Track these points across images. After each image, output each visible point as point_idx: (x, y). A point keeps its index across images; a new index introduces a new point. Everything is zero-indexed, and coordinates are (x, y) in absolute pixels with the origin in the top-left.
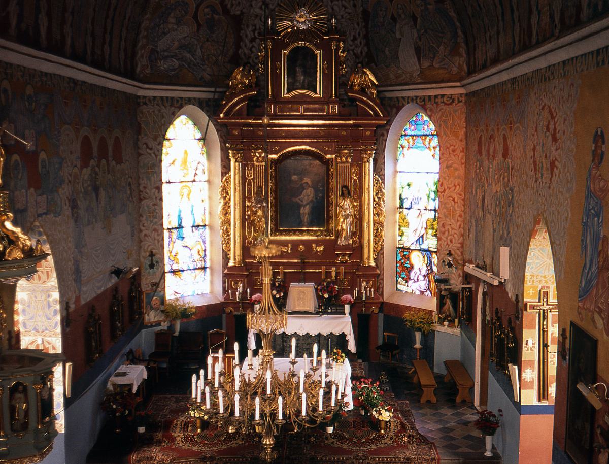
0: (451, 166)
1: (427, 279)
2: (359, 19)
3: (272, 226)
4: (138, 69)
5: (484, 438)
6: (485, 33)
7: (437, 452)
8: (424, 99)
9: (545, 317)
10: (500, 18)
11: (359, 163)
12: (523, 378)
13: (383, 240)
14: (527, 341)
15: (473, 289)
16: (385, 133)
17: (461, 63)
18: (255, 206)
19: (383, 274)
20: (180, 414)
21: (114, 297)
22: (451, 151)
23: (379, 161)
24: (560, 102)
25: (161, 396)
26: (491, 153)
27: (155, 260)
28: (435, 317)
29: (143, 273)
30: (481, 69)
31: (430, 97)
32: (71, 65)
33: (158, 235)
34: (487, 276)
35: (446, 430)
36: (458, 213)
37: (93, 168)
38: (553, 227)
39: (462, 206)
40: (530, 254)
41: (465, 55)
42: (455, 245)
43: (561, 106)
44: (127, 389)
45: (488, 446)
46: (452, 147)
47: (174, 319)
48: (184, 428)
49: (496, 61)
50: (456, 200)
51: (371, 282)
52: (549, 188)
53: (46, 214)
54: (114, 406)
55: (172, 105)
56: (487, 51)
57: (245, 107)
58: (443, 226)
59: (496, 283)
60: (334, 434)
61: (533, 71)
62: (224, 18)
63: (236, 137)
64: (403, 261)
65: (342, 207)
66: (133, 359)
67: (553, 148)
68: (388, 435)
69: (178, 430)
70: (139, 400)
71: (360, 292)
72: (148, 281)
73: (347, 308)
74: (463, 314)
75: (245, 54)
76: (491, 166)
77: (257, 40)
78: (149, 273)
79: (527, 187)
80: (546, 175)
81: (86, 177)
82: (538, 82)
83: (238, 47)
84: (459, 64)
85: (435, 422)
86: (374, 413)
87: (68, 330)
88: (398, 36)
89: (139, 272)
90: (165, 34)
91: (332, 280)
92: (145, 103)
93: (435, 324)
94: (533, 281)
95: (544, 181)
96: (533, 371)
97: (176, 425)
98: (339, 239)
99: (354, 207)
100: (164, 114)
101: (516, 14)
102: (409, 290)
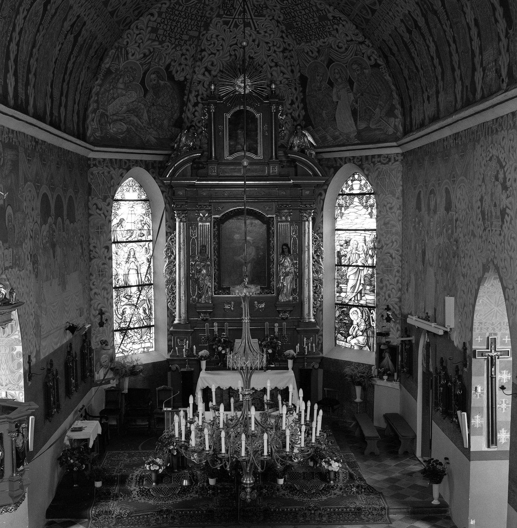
0: (388, 223)
1: (365, 334)
2: (297, 84)
3: (216, 284)
4: (89, 133)
5: (431, 488)
6: (423, 92)
7: (385, 501)
8: (361, 159)
9: (493, 364)
10: (440, 78)
11: (299, 223)
12: (472, 424)
13: (322, 296)
14: (476, 388)
15: (414, 342)
16: (323, 192)
17: (397, 124)
18: (198, 265)
19: (322, 330)
20: (134, 468)
21: (69, 353)
22: (388, 210)
23: (318, 220)
24: (509, 151)
25: (114, 452)
26: (432, 207)
27: (104, 319)
28: (374, 371)
29: (93, 332)
30: (418, 128)
31: (367, 157)
32: (34, 123)
33: (107, 294)
34: (432, 327)
35: (392, 480)
36: (396, 268)
37: (50, 226)
38: (505, 273)
39: (400, 262)
40: (479, 301)
41: (400, 116)
42: (393, 299)
43: (511, 155)
44: (84, 443)
45: (436, 495)
46: (389, 205)
47: (123, 377)
48: (139, 482)
49: (435, 119)
50: (393, 256)
51: (311, 338)
52: (500, 235)
53: (11, 267)
54: (72, 461)
55: (120, 167)
56: (425, 110)
57: (190, 168)
58: (381, 281)
59: (441, 333)
60: (285, 486)
61: (478, 125)
62: (169, 84)
63: (177, 201)
64: (341, 317)
65: (282, 264)
66: (87, 416)
67: (504, 197)
68: (337, 486)
69: (134, 484)
70: (95, 454)
71: (302, 348)
72: (97, 340)
73: (290, 363)
74: (402, 367)
75: (188, 118)
76: (432, 220)
77: (200, 105)
78: (99, 331)
79: (474, 236)
80: (497, 223)
81: (45, 233)
82: (484, 134)
83: (182, 111)
84: (395, 125)
85: (381, 473)
86: (324, 464)
87: (30, 383)
88: (335, 99)
89: (90, 328)
90: (115, 99)
91: (274, 335)
92: (95, 165)
93: (374, 378)
94: (481, 328)
95: (494, 229)
96: (482, 417)
97: (132, 479)
98: (280, 296)
99: (294, 264)
100: (113, 175)
101: (457, 73)
102: (348, 345)
